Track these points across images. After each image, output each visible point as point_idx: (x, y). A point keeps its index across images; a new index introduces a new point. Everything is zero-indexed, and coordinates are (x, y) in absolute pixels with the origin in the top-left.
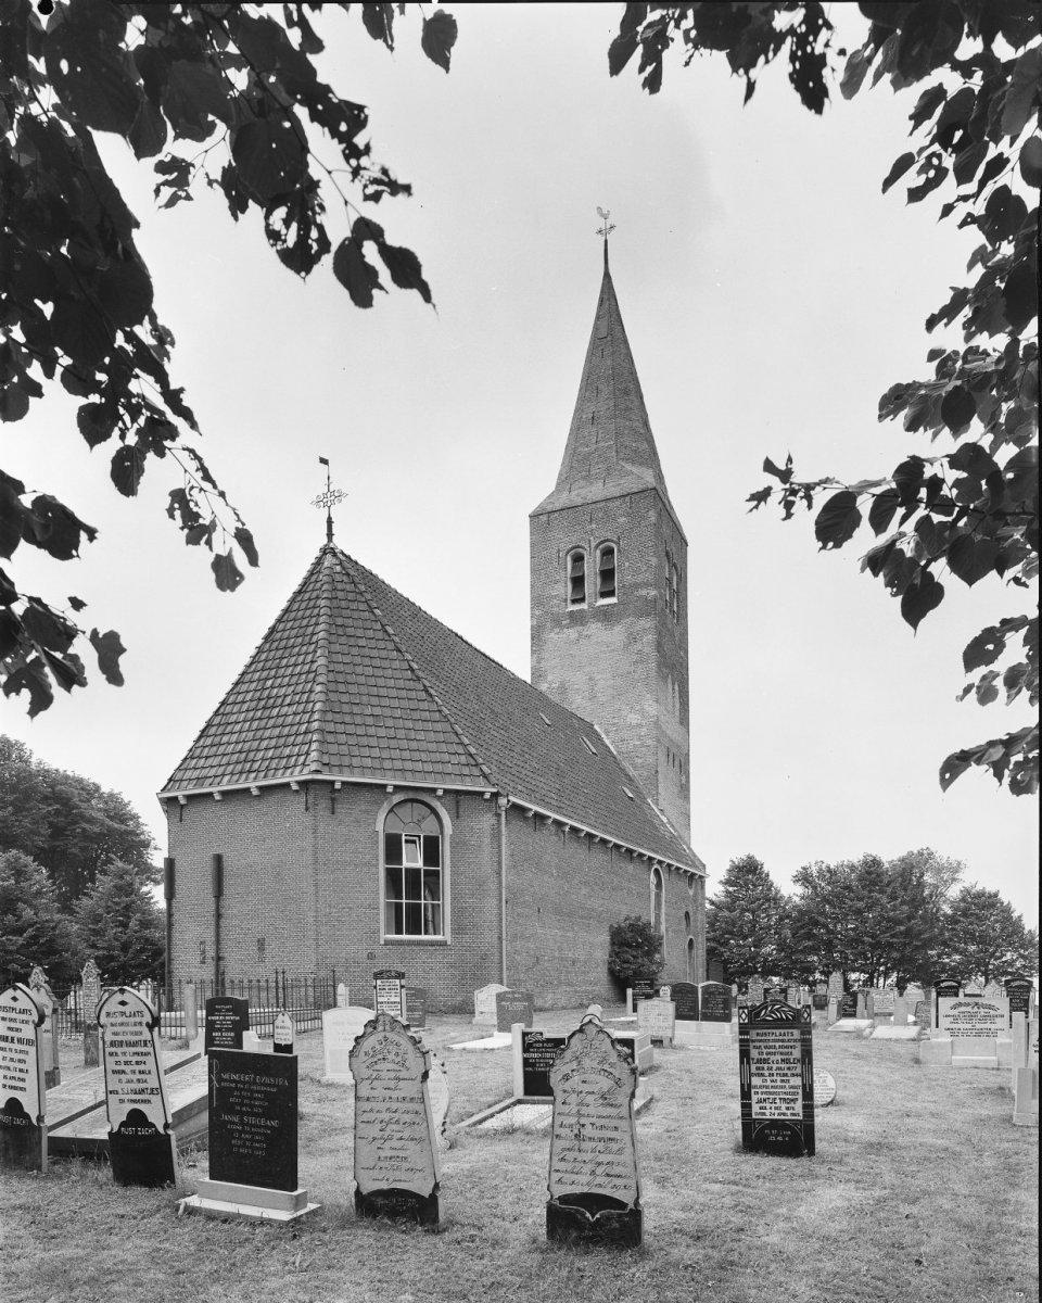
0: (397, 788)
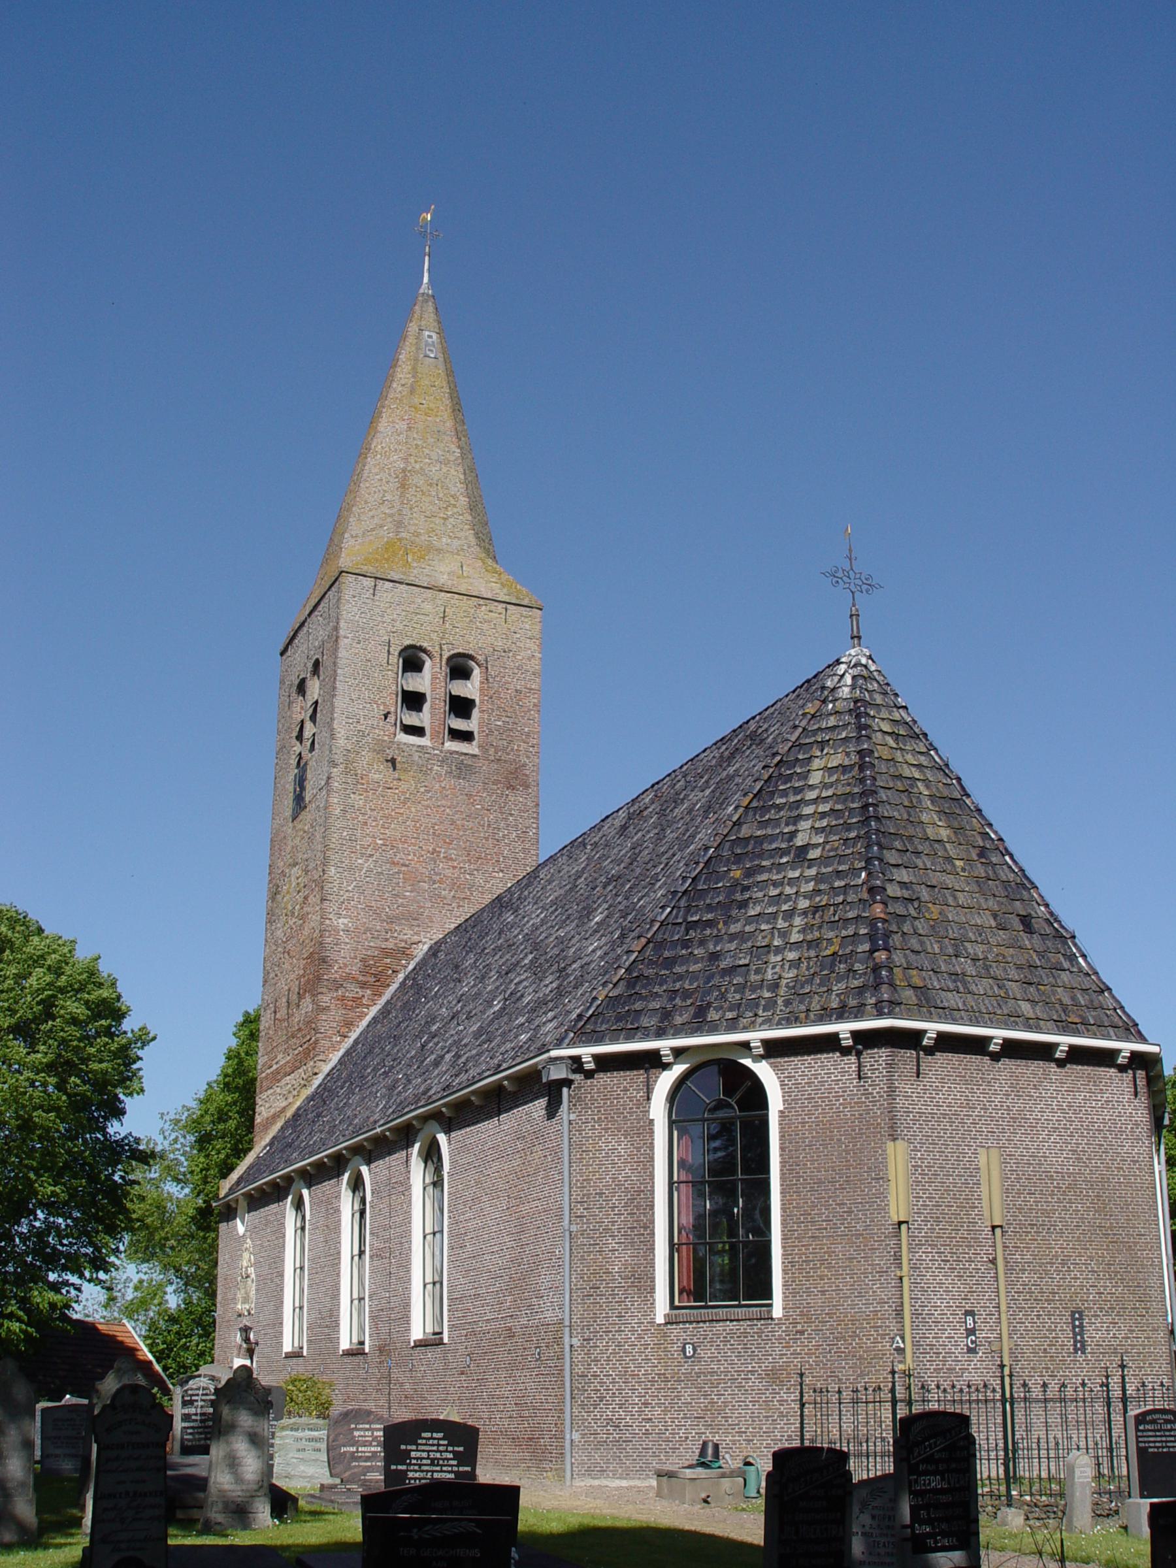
0: (678, 1052)
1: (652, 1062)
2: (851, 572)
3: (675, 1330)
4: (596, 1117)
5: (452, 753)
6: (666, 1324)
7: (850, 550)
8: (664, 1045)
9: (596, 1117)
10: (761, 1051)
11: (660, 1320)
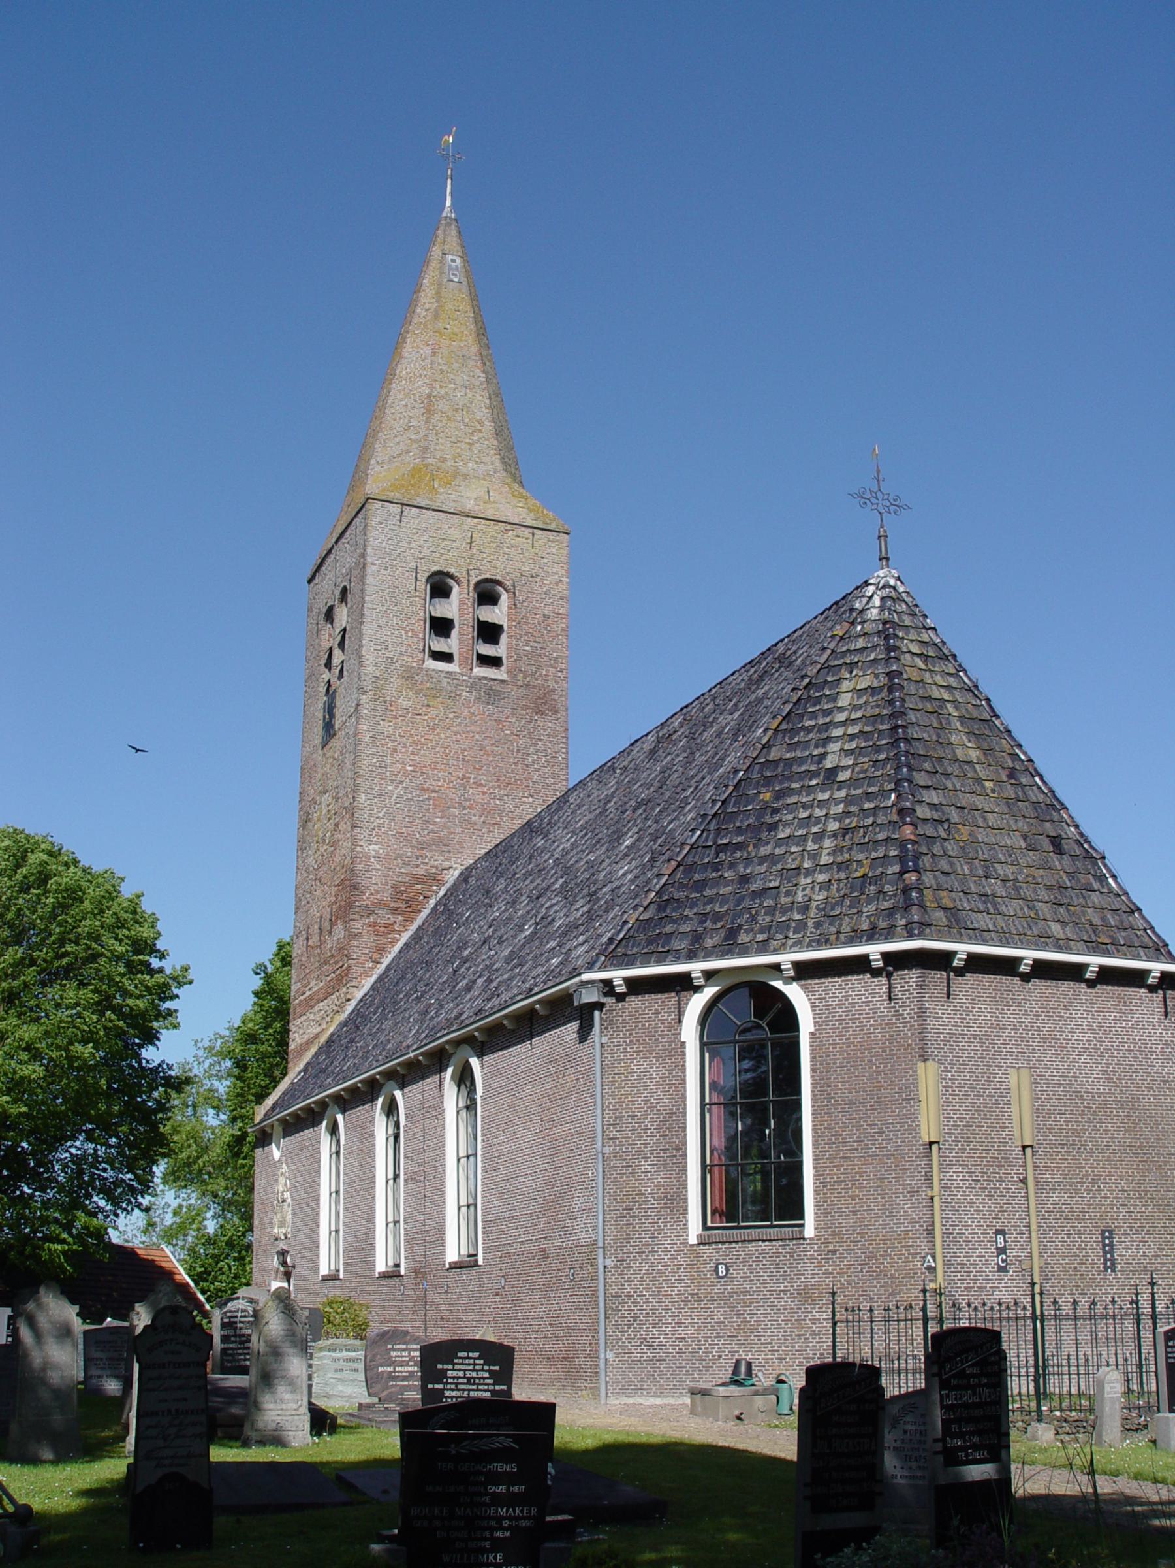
0: (709, 975)
1: (683, 984)
2: (879, 493)
3: (708, 1250)
4: (628, 1040)
5: (480, 678)
6: (699, 1244)
7: (878, 471)
8: (695, 968)
9: (628, 1040)
10: (792, 973)
11: (693, 1240)
